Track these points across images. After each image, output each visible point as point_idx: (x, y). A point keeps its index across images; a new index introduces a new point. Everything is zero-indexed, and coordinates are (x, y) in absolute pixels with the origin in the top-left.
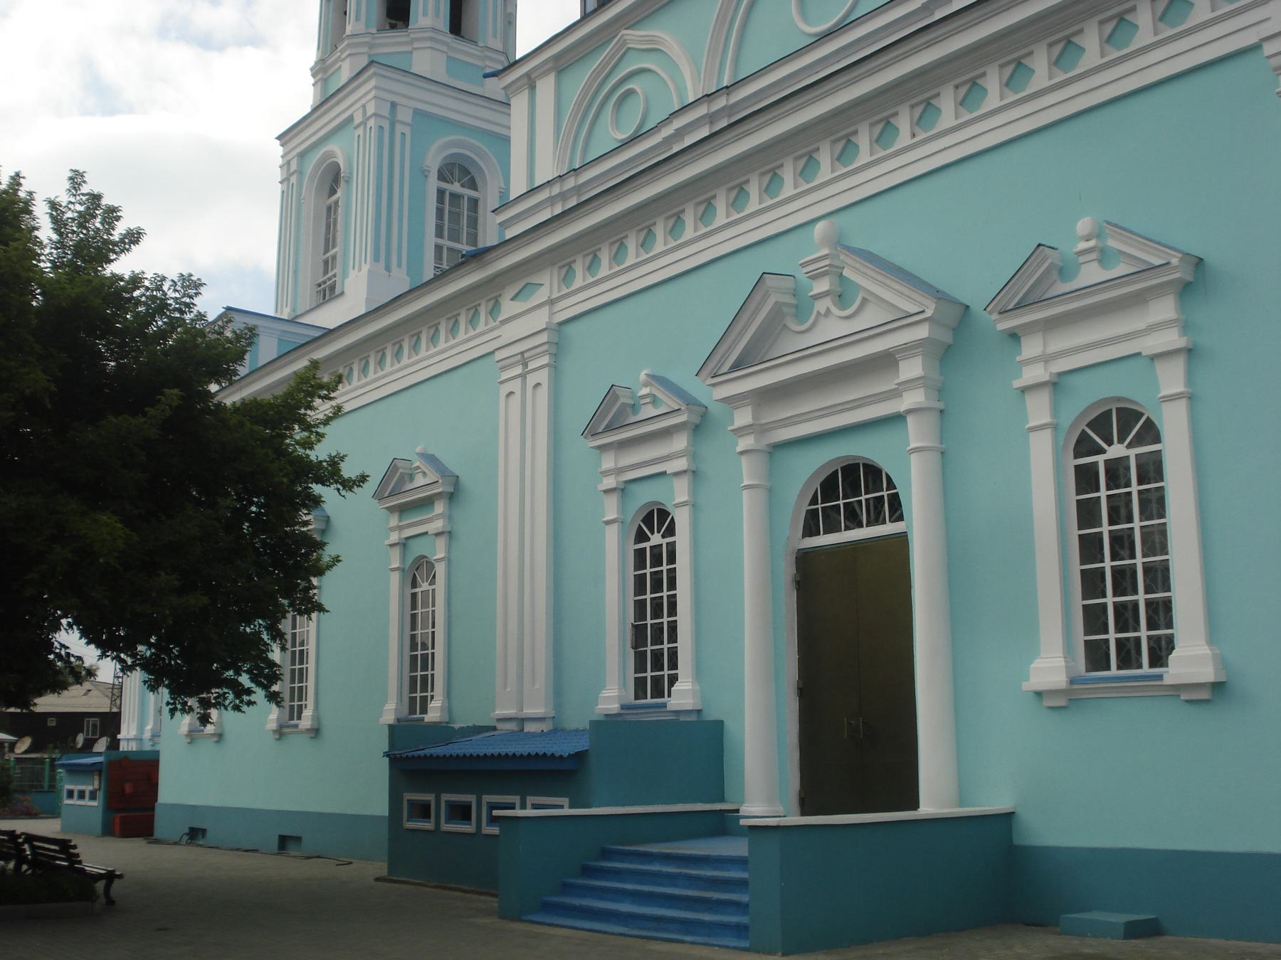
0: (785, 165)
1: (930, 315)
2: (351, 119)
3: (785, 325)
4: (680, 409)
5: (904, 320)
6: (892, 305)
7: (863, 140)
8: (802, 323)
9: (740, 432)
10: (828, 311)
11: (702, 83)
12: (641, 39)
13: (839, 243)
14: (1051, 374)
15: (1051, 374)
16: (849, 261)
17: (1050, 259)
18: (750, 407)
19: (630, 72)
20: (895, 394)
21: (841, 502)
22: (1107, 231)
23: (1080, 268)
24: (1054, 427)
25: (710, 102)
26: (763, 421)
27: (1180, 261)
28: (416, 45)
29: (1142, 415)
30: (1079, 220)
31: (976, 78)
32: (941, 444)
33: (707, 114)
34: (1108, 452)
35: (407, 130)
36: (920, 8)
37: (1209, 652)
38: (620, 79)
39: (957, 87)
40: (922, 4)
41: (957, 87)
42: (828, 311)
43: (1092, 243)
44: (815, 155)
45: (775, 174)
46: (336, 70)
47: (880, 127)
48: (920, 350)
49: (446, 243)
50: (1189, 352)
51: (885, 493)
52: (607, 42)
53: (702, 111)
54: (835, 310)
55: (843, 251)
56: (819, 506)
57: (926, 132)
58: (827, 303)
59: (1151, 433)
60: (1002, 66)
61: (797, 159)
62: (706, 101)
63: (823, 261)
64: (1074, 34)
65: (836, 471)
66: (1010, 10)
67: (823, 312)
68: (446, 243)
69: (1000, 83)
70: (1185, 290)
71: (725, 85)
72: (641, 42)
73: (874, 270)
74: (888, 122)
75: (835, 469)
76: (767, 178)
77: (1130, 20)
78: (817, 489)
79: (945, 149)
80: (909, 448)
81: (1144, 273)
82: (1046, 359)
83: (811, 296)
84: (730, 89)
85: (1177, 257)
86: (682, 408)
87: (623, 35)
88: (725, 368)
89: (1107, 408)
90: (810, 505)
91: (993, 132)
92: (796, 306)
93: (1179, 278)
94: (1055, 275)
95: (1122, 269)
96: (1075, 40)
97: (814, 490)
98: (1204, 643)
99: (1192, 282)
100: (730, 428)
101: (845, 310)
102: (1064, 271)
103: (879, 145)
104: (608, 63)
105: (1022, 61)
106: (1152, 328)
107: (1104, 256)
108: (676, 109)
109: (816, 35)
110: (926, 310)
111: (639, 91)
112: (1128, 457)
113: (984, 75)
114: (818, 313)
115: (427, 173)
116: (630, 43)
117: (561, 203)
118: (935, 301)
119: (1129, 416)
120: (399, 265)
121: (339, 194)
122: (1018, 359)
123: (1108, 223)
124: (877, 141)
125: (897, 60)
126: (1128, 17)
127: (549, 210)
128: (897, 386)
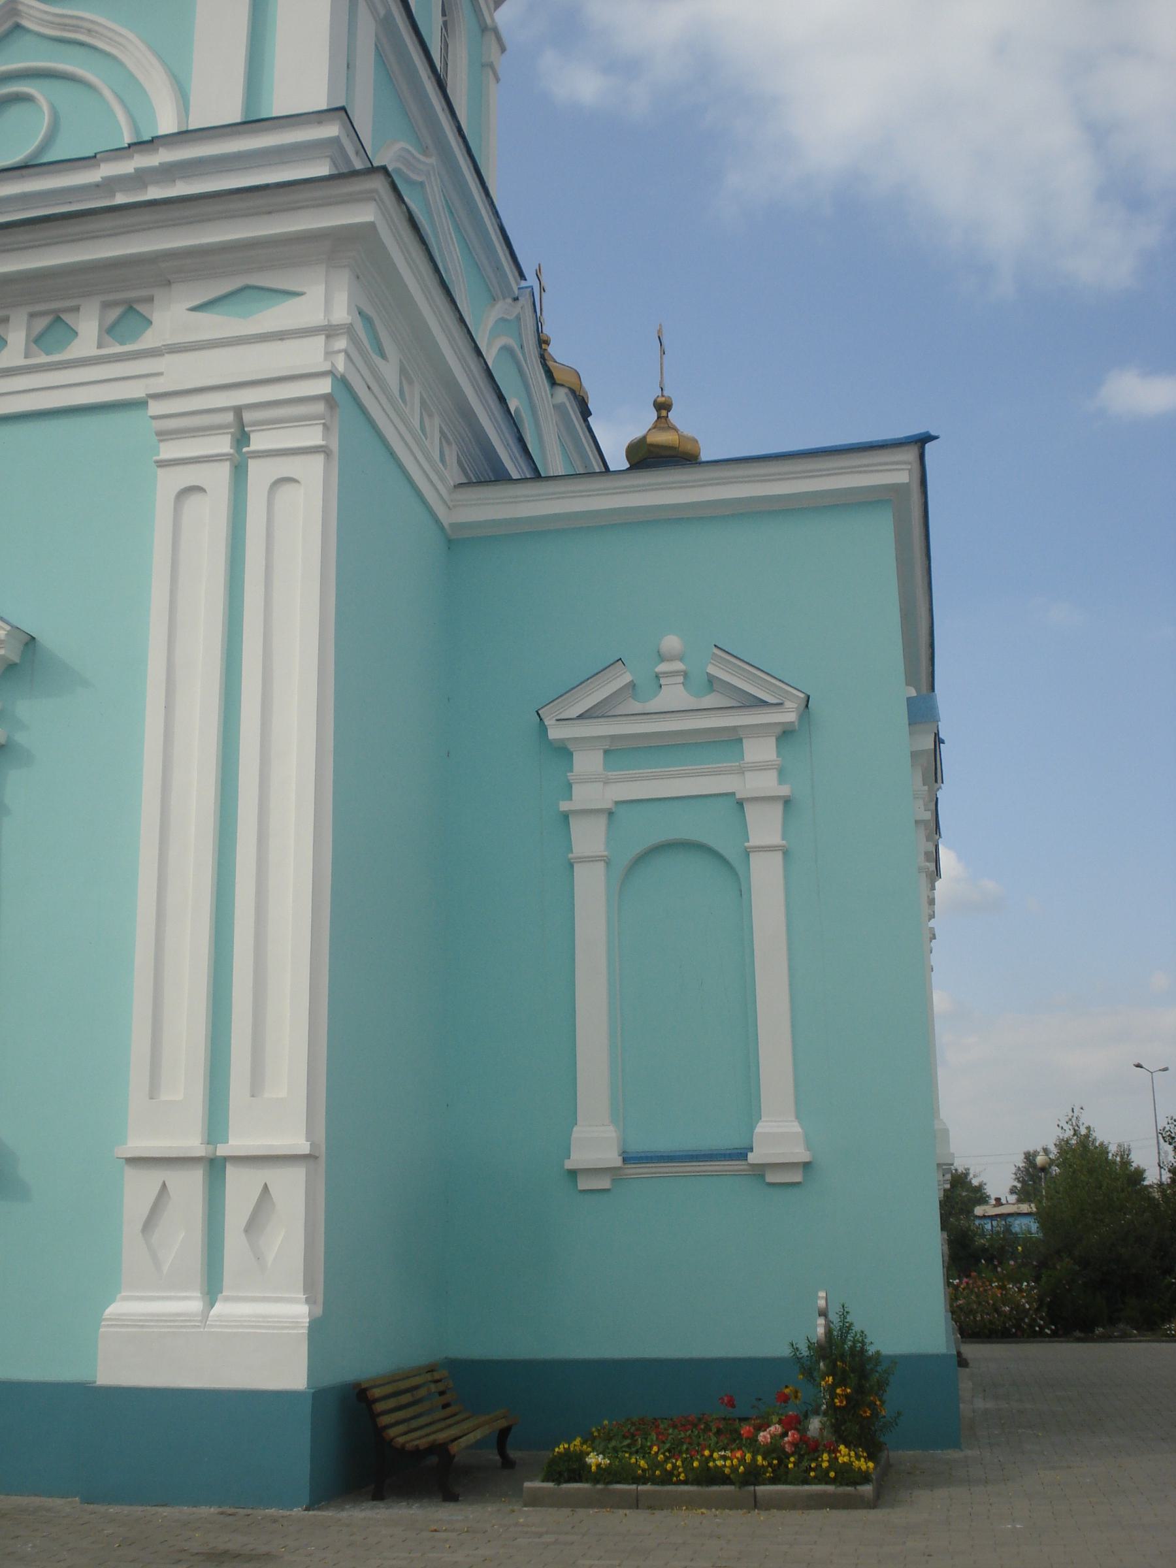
27: (6, 634)
37: (800, 1130)
39: (32, 315)
72: (51, 24)
77: (141, 311)
85: (4, 630)
96: (67, 318)
98: (794, 1119)
99: (16, 664)
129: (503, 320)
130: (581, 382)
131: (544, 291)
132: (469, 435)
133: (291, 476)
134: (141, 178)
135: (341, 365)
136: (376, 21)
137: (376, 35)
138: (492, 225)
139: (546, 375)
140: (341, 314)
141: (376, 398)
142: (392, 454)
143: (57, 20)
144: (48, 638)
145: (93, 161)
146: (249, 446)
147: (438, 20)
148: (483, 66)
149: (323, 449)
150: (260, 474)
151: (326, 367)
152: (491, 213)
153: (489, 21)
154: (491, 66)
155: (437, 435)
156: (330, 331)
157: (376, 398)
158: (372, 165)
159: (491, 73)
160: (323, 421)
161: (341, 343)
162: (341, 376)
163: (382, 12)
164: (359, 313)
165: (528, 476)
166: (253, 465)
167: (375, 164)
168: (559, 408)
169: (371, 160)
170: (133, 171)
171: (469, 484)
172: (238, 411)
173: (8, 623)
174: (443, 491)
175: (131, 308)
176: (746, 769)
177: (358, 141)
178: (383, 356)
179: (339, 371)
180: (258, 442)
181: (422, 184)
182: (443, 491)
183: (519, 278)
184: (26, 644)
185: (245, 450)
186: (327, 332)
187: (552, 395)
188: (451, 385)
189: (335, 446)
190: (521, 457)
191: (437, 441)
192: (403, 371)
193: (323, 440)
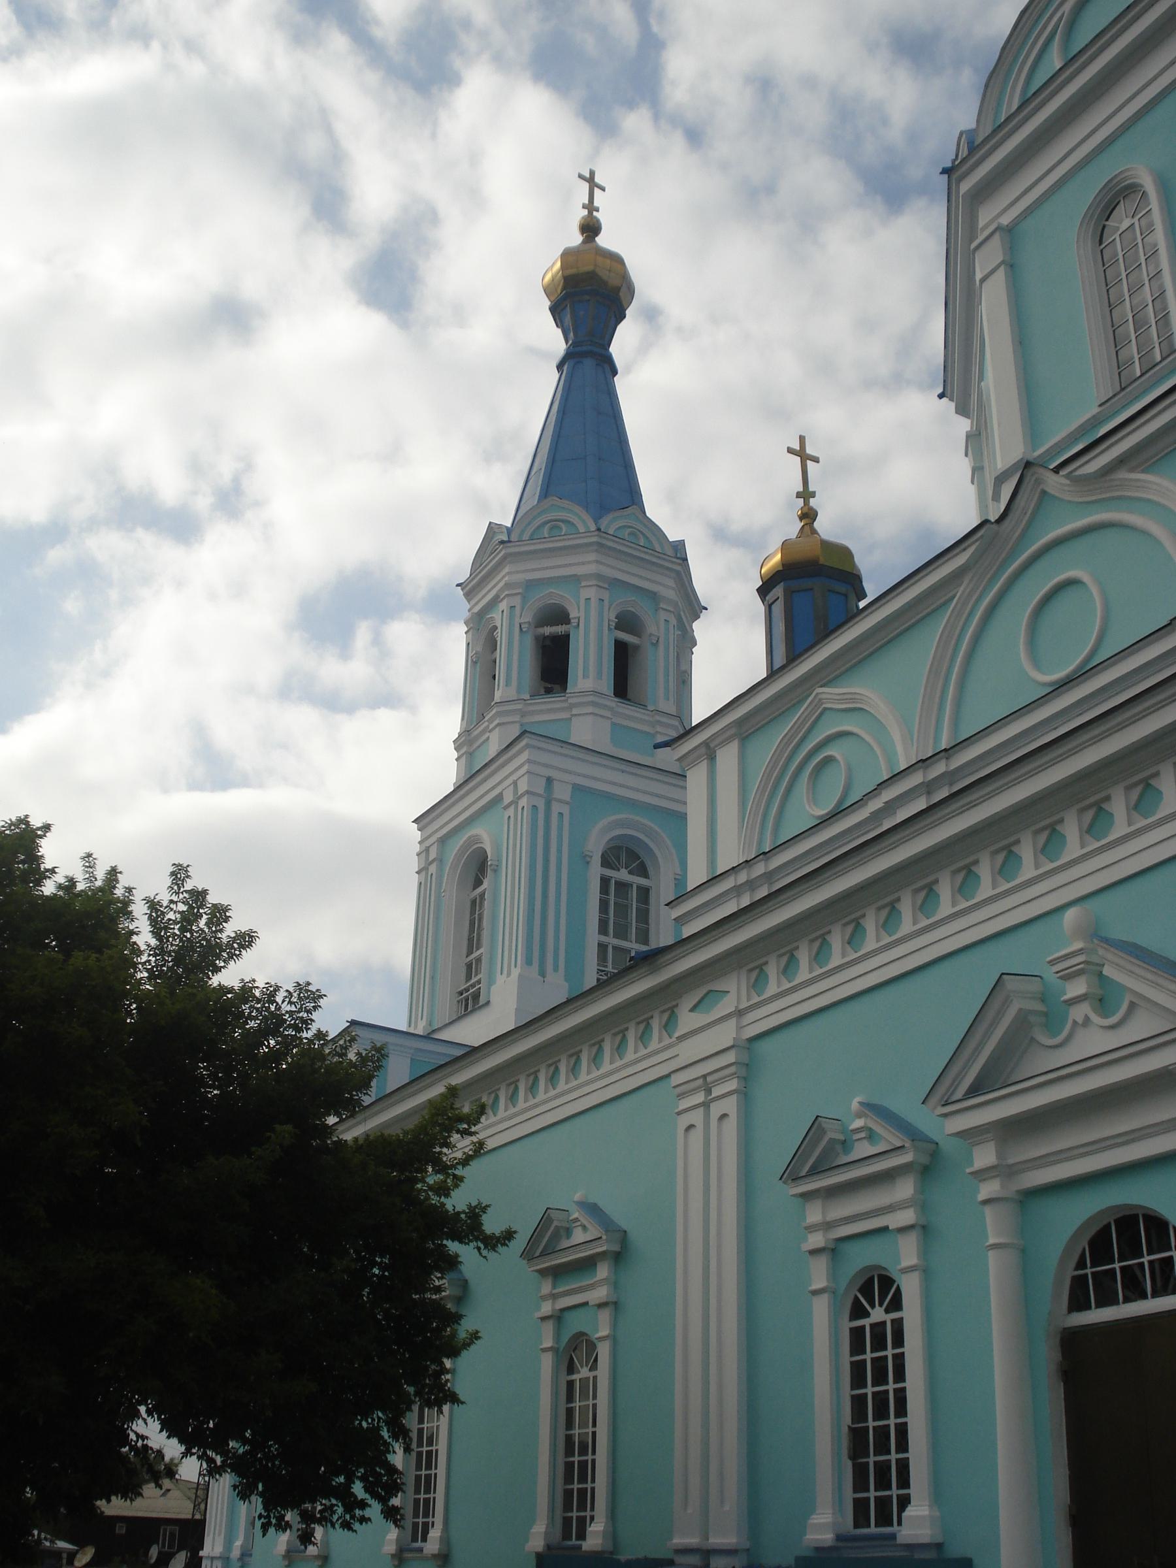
2: (499, 797)
3: (1033, 1039)
8: (1054, 1036)
9: (982, 1175)
13: (1095, 934)
16: (1110, 956)
25: (767, 860)
26: (1011, 1161)
28: (575, 711)
33: (765, 873)
35: (566, 810)
42: (1087, 1021)
46: (484, 742)
49: (612, 941)
53: (916, 779)
54: (1095, 1019)
56: (1089, 1271)
57: (1052, 862)
61: (1037, 832)
63: (1058, 965)
68: (612, 941)
78: (1084, 1250)
82: (828, 1226)
83: (1065, 1002)
87: (817, 694)
88: (959, 1094)
92: (1046, 1014)
94: (838, 1147)
100: (968, 1170)
115: (589, 859)
120: (556, 969)
121: (485, 885)
127: (735, 900)
172: (704, 1077)
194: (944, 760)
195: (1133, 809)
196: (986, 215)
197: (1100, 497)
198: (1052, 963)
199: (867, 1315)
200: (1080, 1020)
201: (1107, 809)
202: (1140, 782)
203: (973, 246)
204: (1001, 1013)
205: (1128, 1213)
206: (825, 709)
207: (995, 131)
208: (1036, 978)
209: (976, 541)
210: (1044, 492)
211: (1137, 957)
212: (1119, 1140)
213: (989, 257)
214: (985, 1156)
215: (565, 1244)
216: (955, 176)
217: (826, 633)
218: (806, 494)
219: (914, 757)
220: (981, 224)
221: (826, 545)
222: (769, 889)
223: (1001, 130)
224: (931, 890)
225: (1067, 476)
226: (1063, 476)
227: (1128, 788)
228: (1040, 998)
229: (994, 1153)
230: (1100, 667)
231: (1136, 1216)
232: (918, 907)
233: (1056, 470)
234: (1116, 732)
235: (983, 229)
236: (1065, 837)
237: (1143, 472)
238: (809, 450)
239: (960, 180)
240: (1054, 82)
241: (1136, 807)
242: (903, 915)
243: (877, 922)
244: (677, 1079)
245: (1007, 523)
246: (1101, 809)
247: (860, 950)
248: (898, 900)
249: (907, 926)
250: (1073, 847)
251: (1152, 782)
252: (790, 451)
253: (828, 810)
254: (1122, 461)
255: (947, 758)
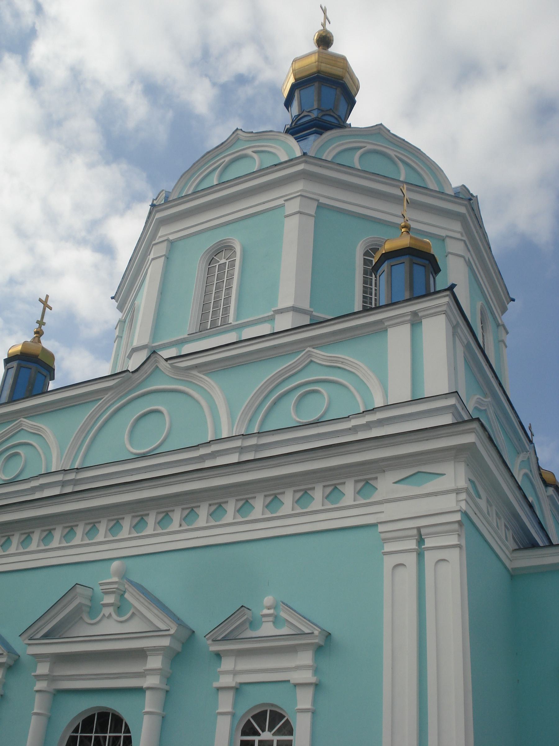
0: (125, 518)
1: (172, 633)
3: (81, 618)
4: (3, 654)
5: (156, 632)
6: (149, 621)
7: (80, 531)
8: (91, 619)
9: (39, 677)
10: (110, 615)
11: (62, 461)
12: (32, 426)
13: (123, 575)
14: (236, 682)
15: (236, 682)
16: (130, 589)
17: (246, 615)
18: (49, 663)
19: (19, 443)
20: (142, 675)
21: (93, 735)
22: (281, 607)
23: (262, 624)
24: (233, 715)
25: (65, 474)
26: (55, 674)
27: (319, 633)
29: (284, 717)
30: (266, 597)
31: (307, 490)
32: (163, 711)
33: (62, 480)
34: (261, 735)
36: (198, 456)
38: (13, 445)
39: (210, 505)
40: (200, 455)
41: (210, 505)
42: (110, 615)
43: (271, 611)
44: (145, 518)
45: (94, 525)
47: (68, 530)
48: (162, 652)
50: (317, 686)
51: (122, 735)
52: (11, 421)
53: (59, 478)
54: (114, 615)
55: (128, 583)
56: (79, 735)
57: (302, 509)
58: (110, 610)
59: (288, 729)
60: (237, 500)
61: (110, 520)
62: (75, 472)
63: (114, 585)
64: (195, 507)
65: (94, 714)
66: (248, 472)
67: (107, 615)
69: (263, 504)
70: (319, 649)
71: (76, 467)
73: (144, 598)
74: (167, 514)
75: (93, 713)
76: (24, 537)
78: (79, 724)
79: (197, 538)
80: (144, 711)
81: (297, 636)
82: (235, 673)
83: (102, 604)
84: (79, 470)
86: (4, 654)
87: (21, 421)
88: (39, 636)
89: (265, 709)
90: (73, 732)
91: (159, 544)
92: (90, 607)
93: (317, 642)
94: (247, 625)
95: (285, 630)
97: (78, 723)
99: (323, 646)
100: (33, 674)
101: (120, 617)
102: (252, 624)
103: (267, 509)
104: (8, 433)
105: (222, 505)
106: (297, 668)
107: (276, 620)
108: (43, 473)
109: (135, 454)
110: (171, 629)
111: (22, 454)
112: (272, 741)
113: (227, 502)
114: (104, 615)
116: (24, 426)
117: (72, 486)
118: (177, 625)
119: (277, 716)
122: (219, 670)
123: (283, 603)
124: (159, 523)
125: (175, 483)
126: (309, 492)
127: (59, 488)
128: (143, 671)
129: (523, 461)
130: (555, 478)
131: (533, 436)
132: (517, 525)
133: (444, 558)
134: (368, 426)
135: (463, 506)
136: (463, 346)
137: (464, 353)
138: (516, 421)
139: (543, 482)
140: (462, 483)
141: (479, 518)
142: (486, 541)
143: (329, 358)
144: (336, 634)
145: (347, 419)
146: (424, 545)
147: (479, 325)
148: (499, 341)
149: (459, 546)
150: (430, 558)
151: (458, 508)
152: (513, 413)
153: (500, 322)
154: (503, 341)
155: (503, 527)
156: (458, 491)
157: (479, 518)
158: (472, 418)
159: (503, 344)
160: (457, 533)
161: (463, 496)
162: (464, 511)
163: (466, 342)
164: (469, 480)
165: (547, 545)
166: (427, 554)
167: (473, 418)
168: (550, 497)
169: (466, 406)
170: (365, 423)
171: (519, 549)
172: (419, 529)
173: (319, 627)
174: (507, 552)
175: (367, 482)
176: (419, 311)
177: (463, 404)
178: (480, 497)
179: (463, 509)
180: (429, 543)
181: (485, 410)
182: (507, 552)
183: (529, 444)
184: (327, 637)
185: (423, 547)
186: (456, 492)
187: (546, 491)
188: (516, 516)
189: (463, 543)
190: (540, 530)
191: (504, 532)
192: (488, 501)
193: (458, 541)
194: (75, 473)
195: (133, 527)
196: (163, 232)
197: (182, 378)
198: (101, 584)
199: (259, 735)
200: (107, 615)
201: (251, 503)
202: (165, 512)
203: (154, 242)
204: (70, 602)
205: (105, 711)
206: (22, 429)
207: (179, 198)
208: (91, 589)
209: (121, 377)
210: (157, 367)
211: (143, 594)
212: (112, 676)
213: (158, 251)
214: (43, 669)
215: (250, 633)
216: (155, 209)
217: (31, 394)
218: (41, 323)
219: (60, 468)
220: (159, 234)
221: (44, 350)
222: (254, 457)
223: (182, 199)
224: (29, 535)
225: (171, 364)
226: (169, 364)
227: (158, 513)
228: (90, 599)
229: (48, 667)
230: (160, 454)
231: (108, 714)
232: (109, 529)
233: (167, 360)
234: (160, 487)
235: (160, 237)
236: (54, 536)
237: (204, 374)
238: (49, 303)
239: (158, 211)
240: (211, 189)
241: (134, 527)
242: (54, 538)
243: (84, 530)
244: (381, 528)
245: (136, 374)
246: (142, 518)
247: (70, 543)
248: (55, 529)
249: (33, 546)
250: (124, 533)
251: (145, 518)
252: (40, 300)
253: (9, 478)
254: (196, 367)
255: (77, 473)
